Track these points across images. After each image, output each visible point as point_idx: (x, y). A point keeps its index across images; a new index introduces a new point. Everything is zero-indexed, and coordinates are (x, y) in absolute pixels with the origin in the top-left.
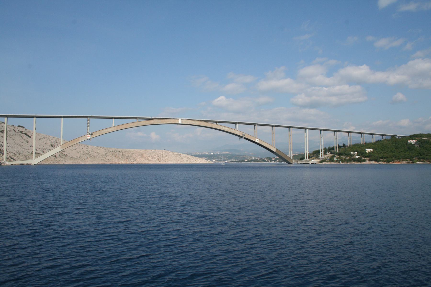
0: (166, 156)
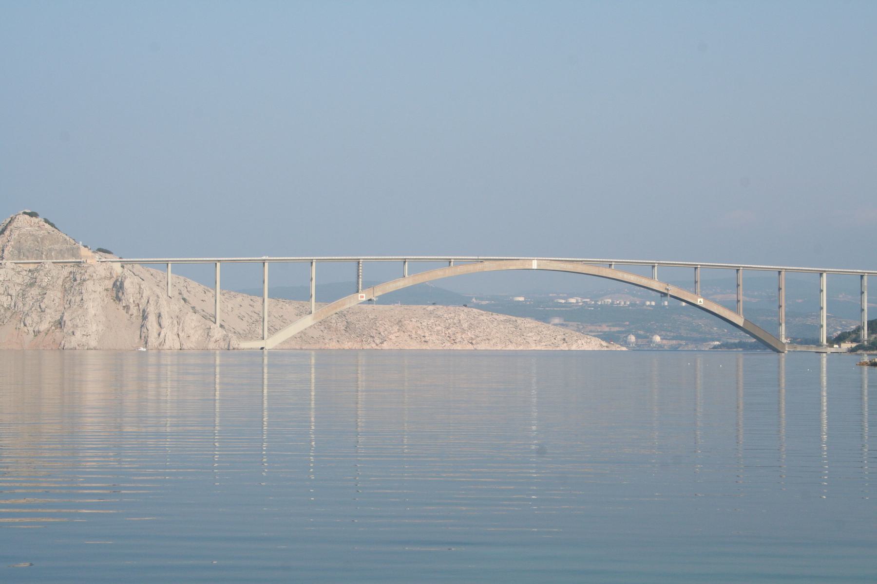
0: (470, 327)
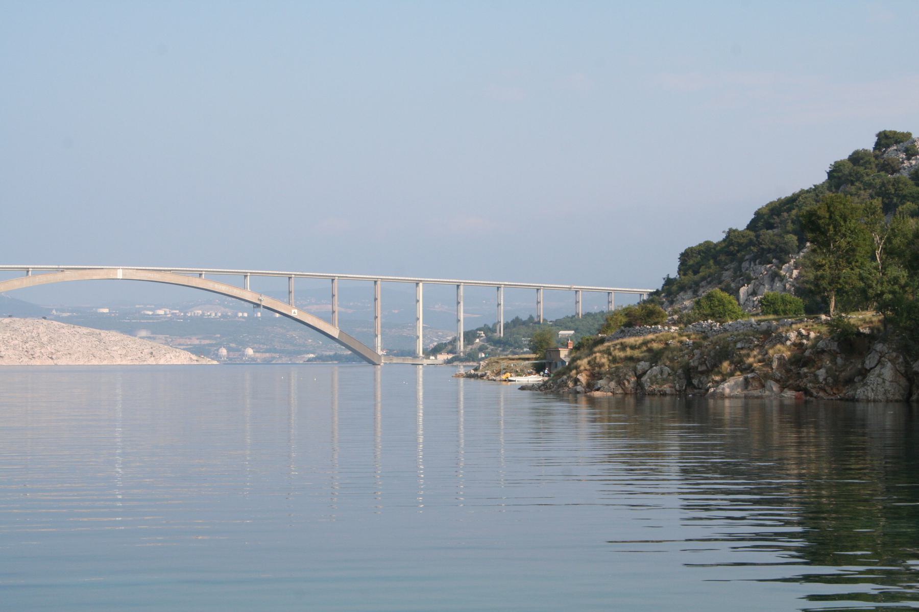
0: (50, 341)
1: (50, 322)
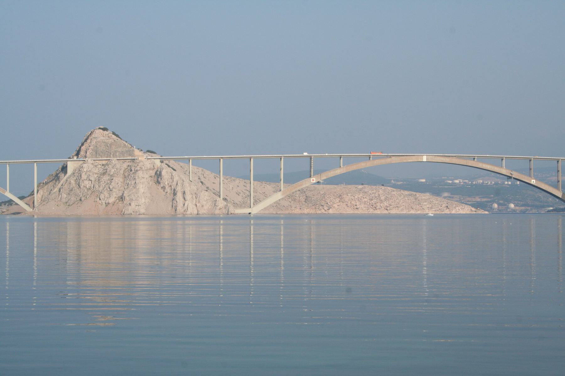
0: (386, 199)
1: (386, 188)
